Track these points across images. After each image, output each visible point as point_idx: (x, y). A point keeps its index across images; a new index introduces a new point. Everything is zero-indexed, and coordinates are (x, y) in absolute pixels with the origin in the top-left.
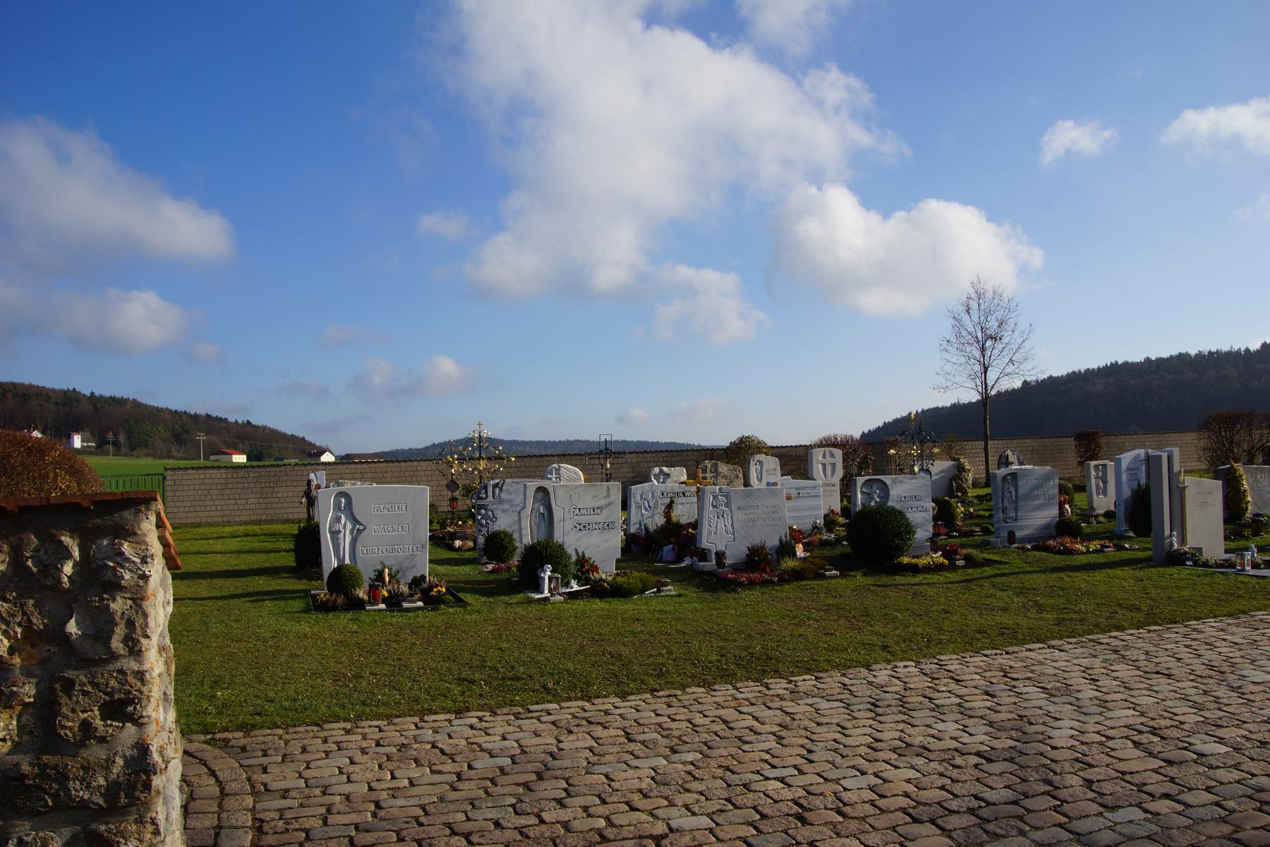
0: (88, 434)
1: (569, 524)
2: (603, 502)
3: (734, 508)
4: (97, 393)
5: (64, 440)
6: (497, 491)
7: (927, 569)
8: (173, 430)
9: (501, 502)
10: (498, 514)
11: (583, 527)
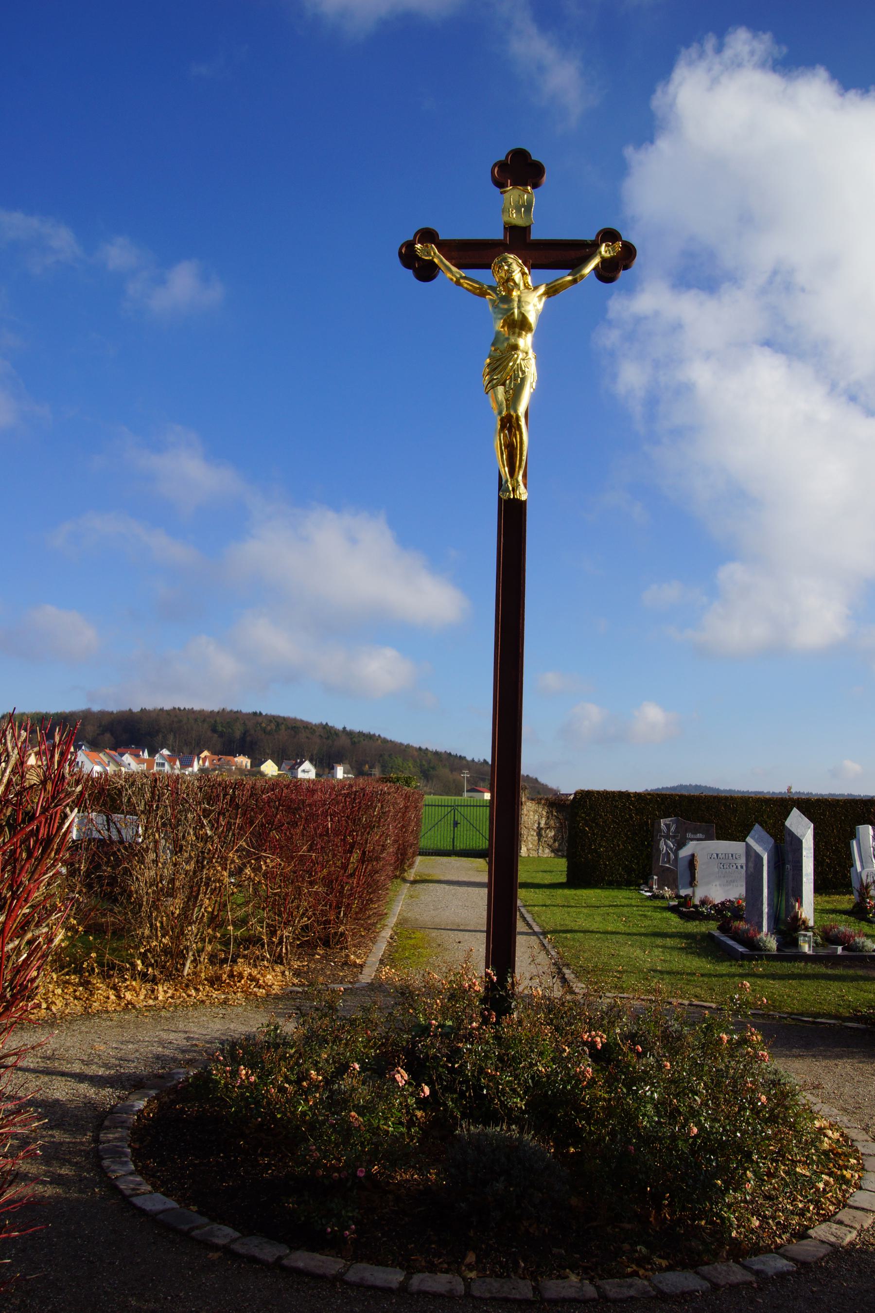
0: (348, 766)
4: (348, 729)
8: (421, 766)
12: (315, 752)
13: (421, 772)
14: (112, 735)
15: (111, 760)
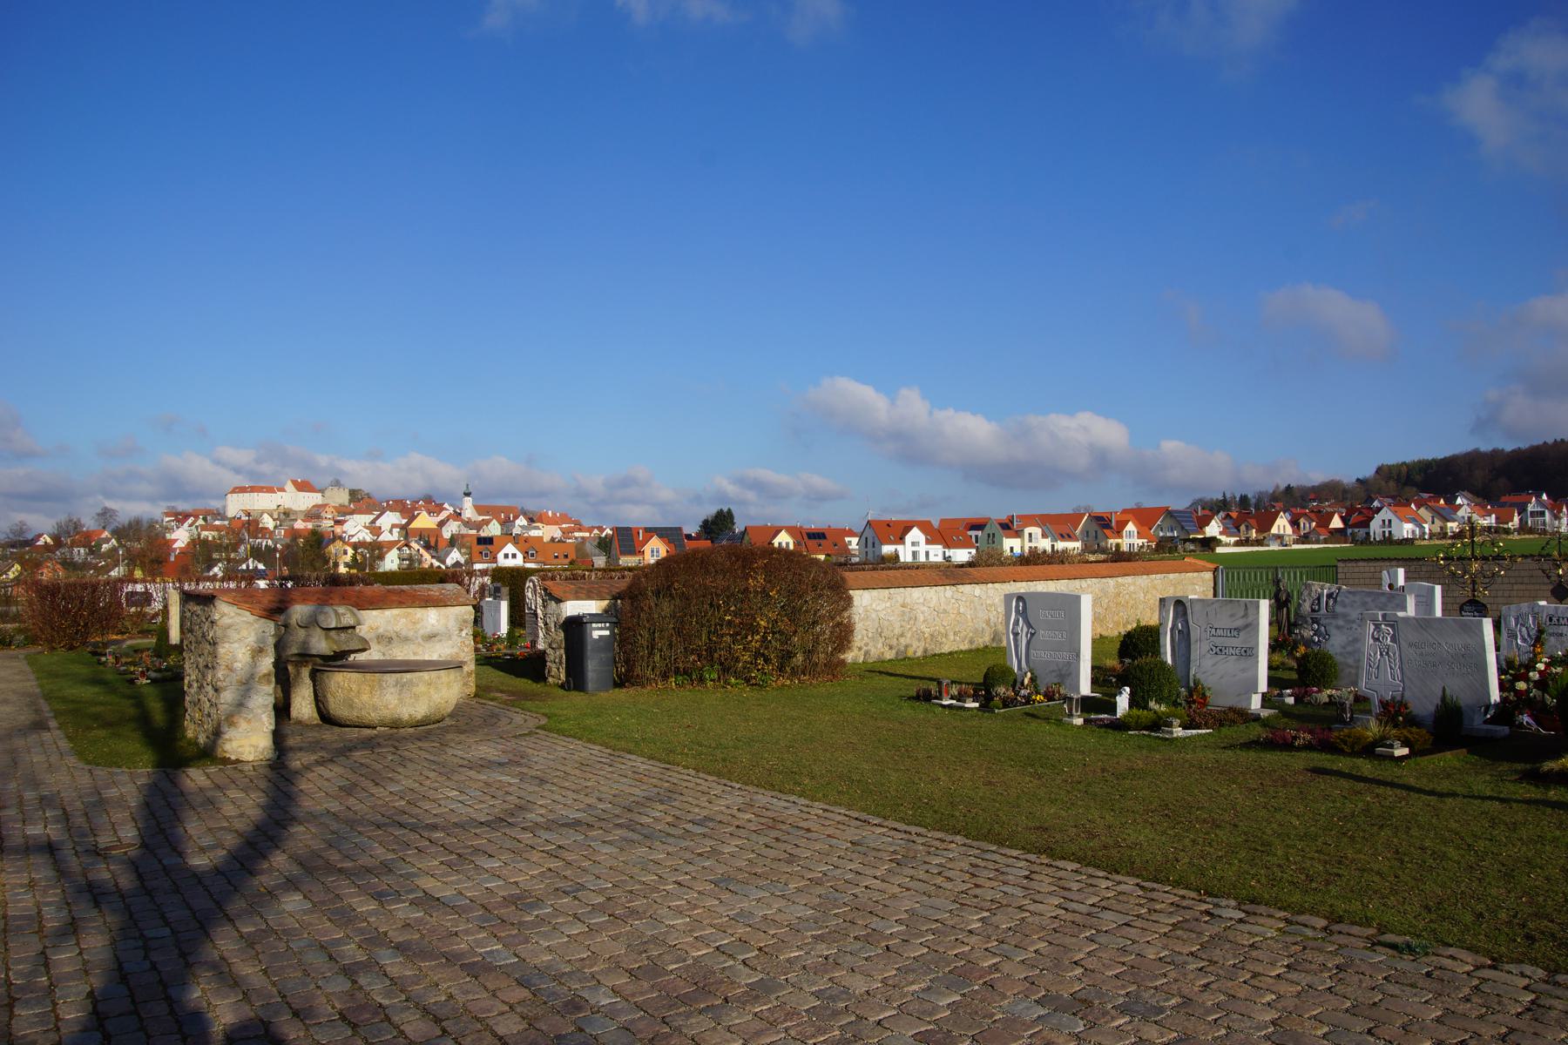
1: (1206, 646)
2: (1240, 623)
9: (1335, 616)
10: (1333, 631)
11: (1219, 651)
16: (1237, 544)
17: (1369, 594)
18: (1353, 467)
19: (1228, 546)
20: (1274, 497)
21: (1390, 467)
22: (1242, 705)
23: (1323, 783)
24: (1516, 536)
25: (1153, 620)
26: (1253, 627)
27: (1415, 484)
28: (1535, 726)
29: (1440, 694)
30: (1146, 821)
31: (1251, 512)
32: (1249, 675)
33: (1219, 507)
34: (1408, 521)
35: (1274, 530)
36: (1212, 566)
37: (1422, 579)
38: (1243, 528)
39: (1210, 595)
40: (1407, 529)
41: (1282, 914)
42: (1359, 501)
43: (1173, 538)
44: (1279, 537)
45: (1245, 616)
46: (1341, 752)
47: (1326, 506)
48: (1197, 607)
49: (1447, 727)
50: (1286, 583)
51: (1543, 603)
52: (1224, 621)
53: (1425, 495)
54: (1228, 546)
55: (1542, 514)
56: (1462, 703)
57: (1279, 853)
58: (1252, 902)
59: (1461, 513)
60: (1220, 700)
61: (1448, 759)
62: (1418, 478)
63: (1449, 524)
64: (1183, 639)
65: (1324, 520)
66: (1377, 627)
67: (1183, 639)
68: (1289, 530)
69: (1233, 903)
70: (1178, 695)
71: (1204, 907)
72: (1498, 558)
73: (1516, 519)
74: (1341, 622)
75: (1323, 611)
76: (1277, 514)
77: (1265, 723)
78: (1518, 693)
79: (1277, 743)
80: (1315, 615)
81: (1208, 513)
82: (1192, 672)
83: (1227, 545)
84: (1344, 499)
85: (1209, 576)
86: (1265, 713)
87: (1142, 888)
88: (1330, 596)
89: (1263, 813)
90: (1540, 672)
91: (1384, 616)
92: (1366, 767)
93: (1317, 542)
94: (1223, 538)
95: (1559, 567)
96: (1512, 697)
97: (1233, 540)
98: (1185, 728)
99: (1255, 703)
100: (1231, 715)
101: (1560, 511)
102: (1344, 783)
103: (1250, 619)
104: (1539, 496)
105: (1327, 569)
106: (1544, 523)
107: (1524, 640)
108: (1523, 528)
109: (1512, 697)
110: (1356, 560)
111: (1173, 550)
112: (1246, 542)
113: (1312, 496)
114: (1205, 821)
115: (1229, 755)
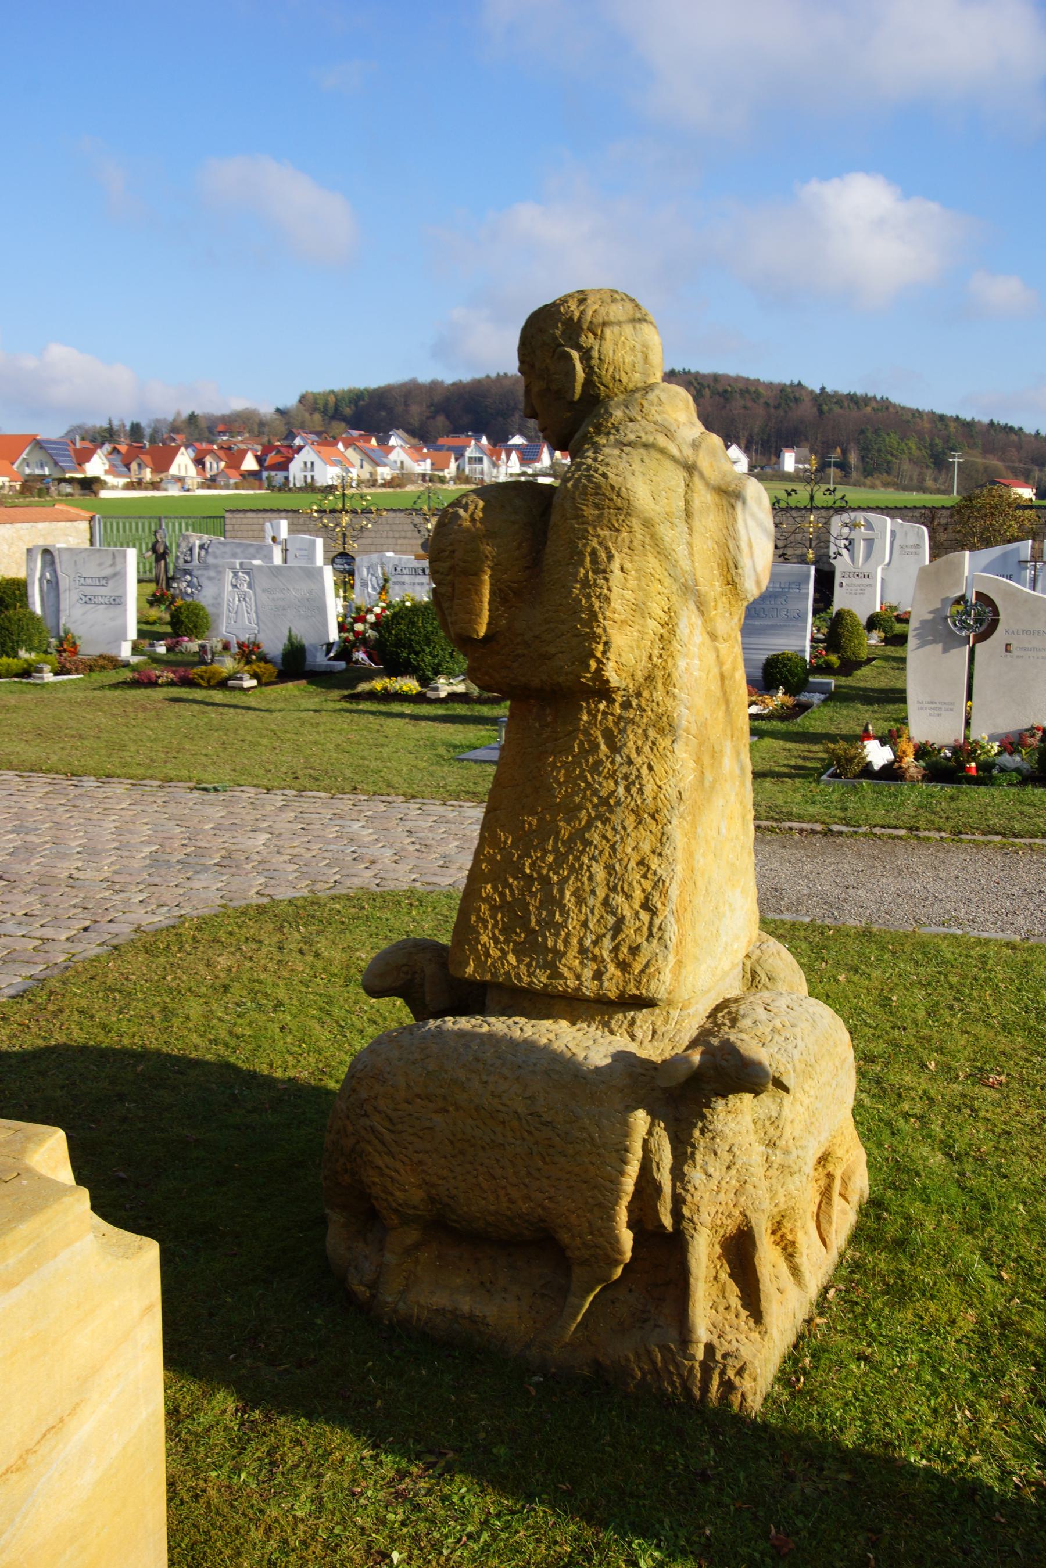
0: (805, 451)
1: (75, 596)
2: (108, 572)
3: (258, 590)
4: (829, 390)
5: (774, 459)
6: (203, 553)
7: (249, 689)
8: (932, 445)
9: (206, 567)
10: (205, 582)
11: (88, 600)
12: (756, 430)
13: (931, 456)
14: (448, 417)
15: (364, 457)
16: (129, 486)
17: (239, 545)
18: (269, 394)
19: (115, 489)
20: (174, 429)
21: (315, 397)
22: (112, 653)
23: (177, 707)
24: (451, 486)
25: (21, 574)
26: (119, 576)
27: (343, 419)
28: (368, 661)
29: (287, 634)
30: (21, 739)
31: (144, 446)
32: (115, 620)
33: (107, 436)
34: (334, 464)
35: (174, 470)
36: (89, 515)
37: (304, 532)
38: (134, 466)
39: (87, 545)
40: (328, 475)
41: (130, 781)
42: (276, 439)
43: (42, 478)
44: (180, 480)
45: (113, 564)
46: (198, 686)
47: (239, 442)
48: (65, 557)
49: (294, 664)
50: (169, 535)
51: (390, 554)
52: (92, 570)
53: (355, 433)
54: (115, 489)
55: (481, 460)
56: (306, 643)
57: (132, 749)
58: (107, 777)
59: (393, 456)
60: (88, 650)
61: (291, 688)
62: (348, 411)
63: (380, 470)
64: (52, 588)
65: (234, 459)
66: (235, 574)
67: (52, 588)
68: (192, 471)
69: (93, 778)
70: (49, 645)
71: (70, 782)
72: (366, 511)
73: (453, 465)
74: (212, 573)
75: (196, 562)
76: (176, 450)
77: (134, 668)
78: (357, 634)
79: (143, 682)
80: (187, 566)
81: (88, 444)
82: (62, 621)
83: (114, 488)
84: (261, 433)
85: (84, 525)
86: (134, 660)
87: (20, 776)
88: (202, 547)
89: (125, 729)
90: (377, 615)
91: (241, 564)
92: (217, 696)
93: (227, 487)
94: (110, 479)
95: (428, 521)
96: (351, 636)
97: (122, 481)
98: (56, 674)
99: (125, 652)
100: (101, 662)
101: (499, 458)
102: (196, 707)
103: (118, 568)
104: (478, 440)
105: (214, 520)
106: (482, 473)
107: (374, 589)
108: (460, 477)
109: (351, 636)
110: (245, 511)
111: (44, 492)
112: (139, 485)
113: (221, 428)
114: (73, 736)
115: (98, 693)
